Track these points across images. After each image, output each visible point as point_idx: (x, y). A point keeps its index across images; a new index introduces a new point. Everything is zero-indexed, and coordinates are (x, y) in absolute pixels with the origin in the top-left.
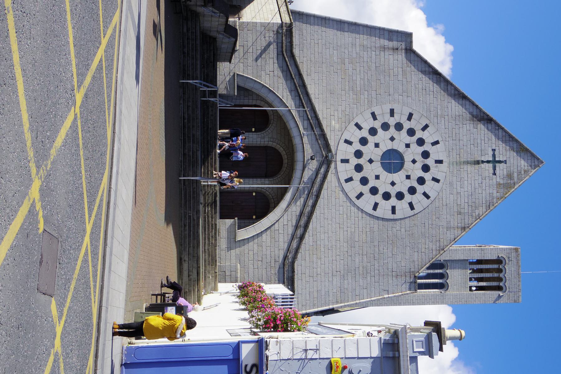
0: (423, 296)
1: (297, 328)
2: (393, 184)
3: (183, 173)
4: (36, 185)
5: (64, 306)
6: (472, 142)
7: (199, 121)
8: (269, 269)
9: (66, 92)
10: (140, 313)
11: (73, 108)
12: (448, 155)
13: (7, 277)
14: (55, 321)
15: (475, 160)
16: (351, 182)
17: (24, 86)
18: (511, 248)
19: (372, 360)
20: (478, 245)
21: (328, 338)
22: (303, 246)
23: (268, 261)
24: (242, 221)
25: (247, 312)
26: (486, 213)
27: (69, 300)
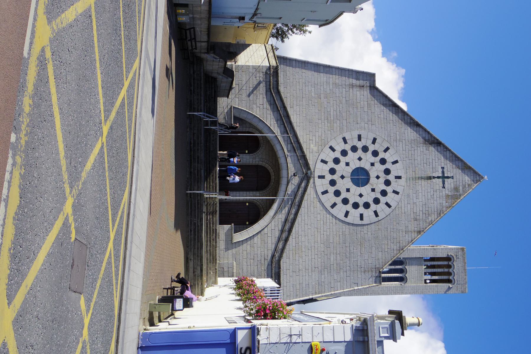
0: (387, 287)
1: (283, 317)
2: (361, 195)
3: (189, 188)
4: (70, 202)
5: (91, 301)
6: (425, 162)
7: (202, 145)
8: (259, 266)
9: (95, 125)
10: (154, 304)
11: (100, 138)
12: (405, 172)
13: (44, 280)
14: (83, 314)
15: (428, 176)
16: (326, 194)
17: (61, 122)
18: (458, 248)
19: (346, 344)
20: (431, 245)
21: (309, 325)
22: (287, 247)
23: (259, 259)
24: (237, 226)
25: (242, 302)
26: (438, 219)
27: (95, 296)
